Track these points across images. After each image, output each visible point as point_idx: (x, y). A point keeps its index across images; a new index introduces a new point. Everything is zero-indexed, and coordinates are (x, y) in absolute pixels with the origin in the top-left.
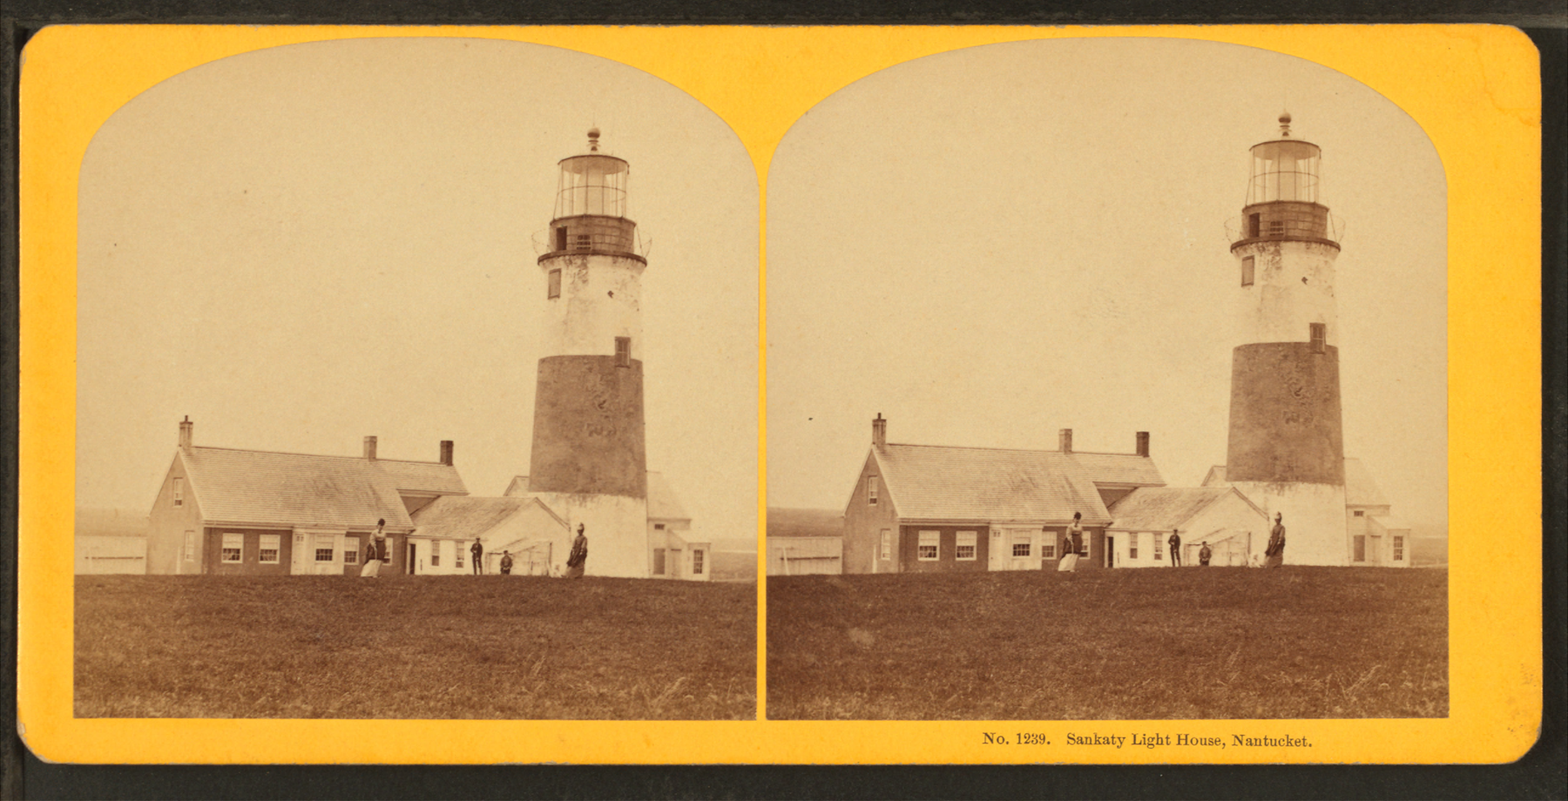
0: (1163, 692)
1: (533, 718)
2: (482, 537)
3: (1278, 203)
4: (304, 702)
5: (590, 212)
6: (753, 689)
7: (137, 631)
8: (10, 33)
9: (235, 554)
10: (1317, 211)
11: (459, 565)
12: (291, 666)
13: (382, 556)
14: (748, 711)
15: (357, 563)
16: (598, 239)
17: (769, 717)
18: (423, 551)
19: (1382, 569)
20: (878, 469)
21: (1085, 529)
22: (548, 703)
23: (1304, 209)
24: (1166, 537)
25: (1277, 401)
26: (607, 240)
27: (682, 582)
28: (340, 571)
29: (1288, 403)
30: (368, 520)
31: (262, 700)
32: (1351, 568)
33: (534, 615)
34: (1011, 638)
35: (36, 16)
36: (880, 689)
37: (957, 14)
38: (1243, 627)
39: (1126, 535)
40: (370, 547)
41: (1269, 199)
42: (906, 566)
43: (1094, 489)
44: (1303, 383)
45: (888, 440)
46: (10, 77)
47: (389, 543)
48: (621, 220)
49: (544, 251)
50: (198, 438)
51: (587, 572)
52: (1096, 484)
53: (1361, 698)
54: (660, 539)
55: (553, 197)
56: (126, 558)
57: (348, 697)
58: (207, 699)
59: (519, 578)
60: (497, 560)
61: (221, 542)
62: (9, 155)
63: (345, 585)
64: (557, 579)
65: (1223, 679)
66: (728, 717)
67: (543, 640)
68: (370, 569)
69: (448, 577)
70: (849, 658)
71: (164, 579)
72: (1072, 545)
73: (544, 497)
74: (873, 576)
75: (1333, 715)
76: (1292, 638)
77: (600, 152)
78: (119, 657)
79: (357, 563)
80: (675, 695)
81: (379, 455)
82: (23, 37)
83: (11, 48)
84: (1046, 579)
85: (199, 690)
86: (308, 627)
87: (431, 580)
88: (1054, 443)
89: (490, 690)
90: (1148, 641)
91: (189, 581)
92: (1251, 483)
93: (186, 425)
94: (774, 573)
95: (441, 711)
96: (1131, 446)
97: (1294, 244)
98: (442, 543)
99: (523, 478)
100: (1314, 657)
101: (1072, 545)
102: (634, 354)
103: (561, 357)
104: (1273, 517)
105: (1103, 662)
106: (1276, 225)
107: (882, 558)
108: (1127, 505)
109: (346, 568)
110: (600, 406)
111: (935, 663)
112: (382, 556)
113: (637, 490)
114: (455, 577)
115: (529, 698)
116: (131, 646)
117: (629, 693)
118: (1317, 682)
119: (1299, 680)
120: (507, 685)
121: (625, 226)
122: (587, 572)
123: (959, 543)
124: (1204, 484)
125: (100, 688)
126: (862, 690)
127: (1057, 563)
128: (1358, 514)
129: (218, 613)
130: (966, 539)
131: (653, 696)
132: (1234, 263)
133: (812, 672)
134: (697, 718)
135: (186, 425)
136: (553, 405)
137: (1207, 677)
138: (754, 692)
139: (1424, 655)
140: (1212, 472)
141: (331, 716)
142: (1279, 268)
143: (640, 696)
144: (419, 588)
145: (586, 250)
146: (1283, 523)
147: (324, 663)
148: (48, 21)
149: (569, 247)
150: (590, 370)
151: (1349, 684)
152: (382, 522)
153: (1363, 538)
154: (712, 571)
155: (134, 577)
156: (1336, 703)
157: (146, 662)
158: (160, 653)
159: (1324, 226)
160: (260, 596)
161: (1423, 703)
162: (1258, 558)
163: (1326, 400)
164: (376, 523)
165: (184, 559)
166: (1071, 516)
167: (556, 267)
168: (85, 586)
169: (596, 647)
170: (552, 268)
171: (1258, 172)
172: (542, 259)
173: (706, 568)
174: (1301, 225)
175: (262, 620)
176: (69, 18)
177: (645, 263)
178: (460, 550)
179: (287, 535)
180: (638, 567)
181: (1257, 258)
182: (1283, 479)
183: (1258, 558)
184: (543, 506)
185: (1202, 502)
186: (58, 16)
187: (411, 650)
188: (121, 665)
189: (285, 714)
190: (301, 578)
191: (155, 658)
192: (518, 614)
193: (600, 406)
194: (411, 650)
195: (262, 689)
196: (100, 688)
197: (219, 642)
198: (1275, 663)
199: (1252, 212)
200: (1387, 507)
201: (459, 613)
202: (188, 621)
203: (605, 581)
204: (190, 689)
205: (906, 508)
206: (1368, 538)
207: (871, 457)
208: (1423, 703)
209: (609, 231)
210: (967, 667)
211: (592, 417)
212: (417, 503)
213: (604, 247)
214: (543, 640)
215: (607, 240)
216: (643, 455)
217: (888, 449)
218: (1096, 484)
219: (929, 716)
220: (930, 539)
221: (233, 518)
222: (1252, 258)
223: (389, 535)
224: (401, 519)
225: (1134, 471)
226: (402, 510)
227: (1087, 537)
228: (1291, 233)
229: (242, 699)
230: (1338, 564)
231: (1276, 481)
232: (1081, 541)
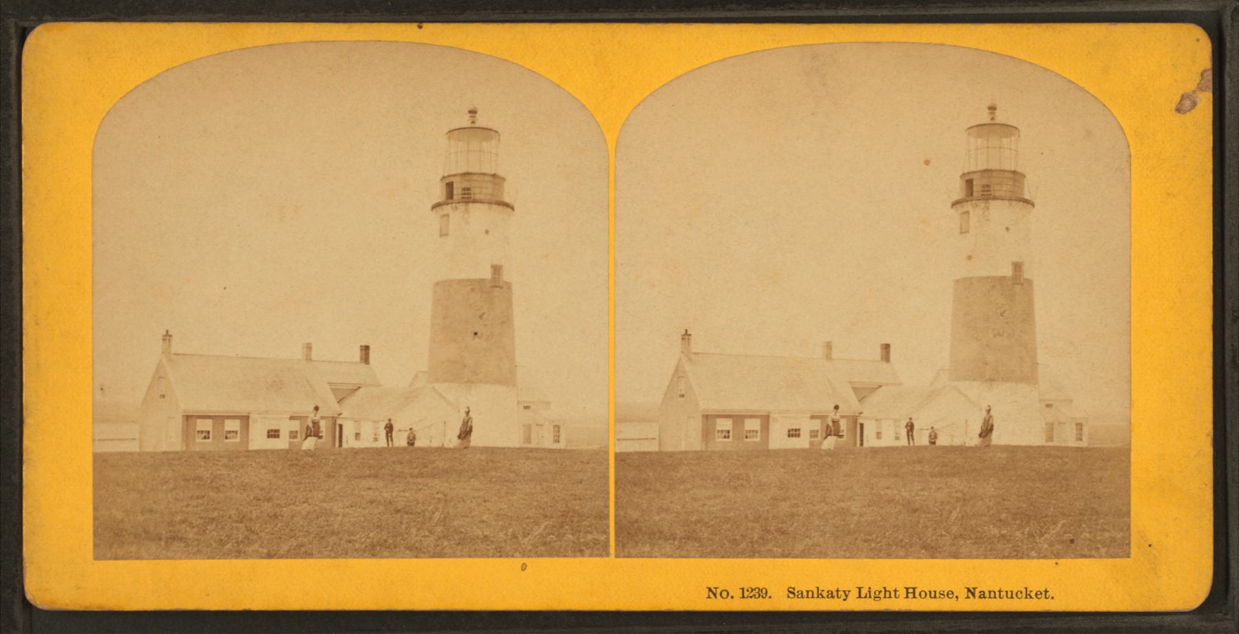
0: (901, 541)
1: (434, 556)
2: (914, 417)
5: (471, 170)
10: (1016, 176)
11: (376, 440)
12: (251, 520)
13: (317, 434)
15: (819, 439)
16: (477, 191)
17: (617, 556)
18: (348, 431)
21: (842, 417)
22: (446, 543)
23: (1006, 175)
24: (904, 423)
26: (484, 191)
28: (807, 446)
29: (1000, 311)
31: (228, 546)
33: (953, 475)
34: (269, 500)
36: (174, 539)
38: (962, 492)
39: (873, 422)
41: (980, 168)
43: (328, 388)
45: (173, 351)
47: (323, 424)
48: (1014, 172)
49: (957, 197)
52: (851, 383)
53: (1051, 544)
55: (437, 161)
57: (294, 542)
58: (187, 545)
60: (927, 433)
61: (195, 424)
62: (14, 123)
63: (291, 458)
64: (971, 448)
67: (440, 496)
69: (888, 448)
70: (663, 515)
71: (153, 455)
73: (441, 387)
74: (682, 453)
75: (1029, 557)
76: (480, 500)
77: (477, 125)
78: (119, 515)
79: (819, 439)
80: (541, 535)
81: (314, 357)
82: (23, 35)
83: (14, 42)
86: (262, 489)
87: (355, 452)
89: (401, 534)
90: (371, 502)
91: (172, 456)
92: (446, 384)
93: (167, 336)
94: (618, 450)
95: (365, 551)
96: (878, 353)
97: (998, 202)
100: (1015, 514)
101: (833, 430)
102: (506, 277)
105: (339, 518)
107: (687, 439)
108: (875, 398)
109: (290, 444)
110: (481, 317)
111: (729, 519)
112: (317, 434)
114: (551, 451)
118: (1018, 534)
120: (414, 531)
125: (112, 538)
126: (674, 539)
127: (301, 444)
129: (194, 480)
130: (752, 425)
131: (525, 536)
132: (434, 218)
135: (167, 336)
137: (418, 530)
139: (1097, 513)
140: (416, 376)
141: (282, 557)
143: (514, 536)
144: (346, 458)
145: (988, 195)
146: (992, 413)
148: (41, 21)
149: (455, 197)
151: (1042, 535)
152: (317, 408)
155: (130, 454)
156: (1032, 549)
158: (151, 511)
159: (1023, 188)
160: (225, 466)
161: (1097, 549)
162: (973, 440)
164: (832, 408)
165: (170, 439)
166: (311, 408)
167: (965, 209)
169: (480, 500)
172: (955, 204)
175: (227, 484)
177: (1033, 205)
179: (245, 419)
180: (1033, 437)
181: (452, 216)
182: (470, 382)
183: (973, 440)
186: (48, 17)
187: (340, 505)
188: (122, 521)
189: (761, 555)
190: (257, 452)
194: (340, 505)
195: (229, 537)
196: (112, 538)
197: (194, 503)
198: (986, 519)
199: (448, 181)
201: (376, 476)
204: (174, 538)
207: (680, 359)
208: (1097, 549)
211: (477, 315)
212: (344, 394)
215: (484, 191)
218: (851, 383)
220: (726, 424)
221: (203, 408)
222: (968, 212)
224: (330, 406)
226: (332, 400)
227: (843, 425)
228: (997, 194)
229: (214, 545)
230: (511, 445)
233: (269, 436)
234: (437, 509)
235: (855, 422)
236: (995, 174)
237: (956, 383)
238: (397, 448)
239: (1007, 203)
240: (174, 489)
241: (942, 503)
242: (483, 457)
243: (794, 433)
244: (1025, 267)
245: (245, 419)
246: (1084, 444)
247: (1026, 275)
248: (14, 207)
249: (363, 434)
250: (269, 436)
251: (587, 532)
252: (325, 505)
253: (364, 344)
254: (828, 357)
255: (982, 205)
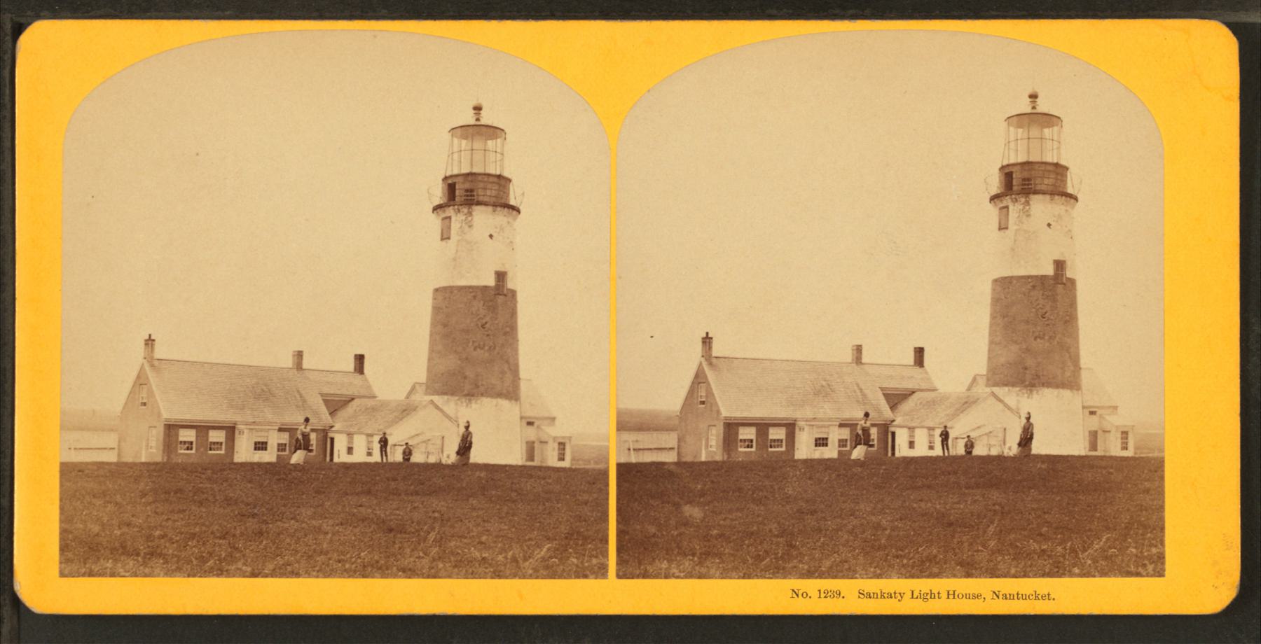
1: (428, 577)
2: (388, 432)
3: (1028, 163)
4: (244, 564)
5: (475, 170)
6: (605, 554)
7: (110, 507)
8: (8, 27)
9: (189, 445)
10: (1059, 170)
11: (369, 454)
12: (234, 535)
13: (307, 447)
14: (601, 572)
15: (287, 453)
16: (481, 192)
17: (619, 577)
18: (340, 443)
19: (1111, 457)
20: (706, 377)
21: (873, 425)
24: (938, 432)
25: (1027, 322)
26: (488, 193)
27: (549, 468)
29: (1036, 324)
30: (296, 418)
31: (211, 563)
32: (1086, 457)
34: (813, 513)
35: (29, 13)
36: (707, 554)
37: (769, 11)
39: (906, 430)
40: (297, 440)
41: (1020, 160)
42: (729, 455)
44: (1048, 308)
46: (9, 62)
47: (313, 436)
48: (499, 177)
49: (437, 201)
50: (160, 352)
51: (472, 460)
52: (882, 389)
53: (1095, 561)
54: (531, 434)
56: (101, 449)
57: (280, 561)
59: (417, 465)
61: (177, 435)
63: (277, 470)
64: (448, 466)
65: (984, 546)
66: (586, 577)
67: (436, 515)
68: (298, 457)
69: (360, 464)
70: (682, 529)
72: (862, 438)
75: (1072, 575)
76: (1039, 513)
77: (483, 122)
78: (96, 529)
79: (287, 453)
80: (543, 559)
81: (304, 366)
82: (19, 30)
83: (8, 38)
84: (841, 465)
85: (160, 555)
86: (248, 504)
87: (347, 467)
88: (848, 356)
89: (394, 555)
90: (923, 515)
92: (1006, 389)
94: (623, 460)
95: (355, 572)
96: (910, 358)
97: (1040, 197)
98: (355, 437)
99: (421, 384)
100: (1057, 528)
101: (862, 438)
102: (510, 285)
103: (451, 287)
104: (1024, 416)
105: (887, 532)
106: (1026, 181)
107: (709, 448)
109: (278, 457)
110: (483, 326)
112: (307, 447)
113: (512, 394)
115: (426, 561)
116: (105, 519)
117: (506, 558)
118: (1059, 549)
119: (1044, 547)
120: (408, 551)
121: (503, 182)
122: (472, 460)
123: (771, 437)
124: (969, 389)
125: (81, 553)
126: (694, 555)
127: (850, 453)
128: (1092, 413)
129: (176, 493)
130: (777, 434)
131: (525, 559)
132: (992, 211)
133: (653, 540)
134: (560, 577)
136: (445, 326)
138: (607, 556)
141: (266, 576)
142: (1028, 216)
143: (515, 560)
144: (337, 472)
145: (471, 201)
147: (261, 533)
148: (38, 17)
149: (457, 199)
150: (475, 297)
151: (1085, 550)
152: (307, 420)
153: (1096, 432)
154: (573, 459)
156: (1074, 565)
157: (118, 532)
158: (129, 525)
159: (1065, 184)
160: (209, 479)
161: (1144, 566)
162: (1012, 449)
163: (1066, 322)
164: (302, 420)
166: (861, 415)
168: (68, 471)
169: (479, 520)
170: (444, 215)
171: (1012, 138)
172: (436, 209)
173: (568, 457)
174: (1046, 181)
175: (211, 498)
176: (56, 15)
177: (519, 211)
178: (370, 442)
181: (1011, 208)
182: (1033, 385)
183: (1012, 449)
184: (437, 407)
185: (967, 404)
187: (331, 522)
189: (229, 574)
190: (243, 465)
191: (125, 529)
192: (417, 493)
193: (483, 326)
195: (211, 554)
196: (81, 553)
199: (1007, 171)
200: (1116, 408)
201: (369, 492)
202: (151, 499)
203: (486, 467)
204: (153, 554)
205: (729, 408)
206: (1100, 434)
207: (700, 368)
208: (1144, 566)
209: (489, 186)
210: (777, 536)
211: (476, 335)
213: (486, 199)
214: (436, 515)
215: (488, 193)
216: (517, 365)
217: (714, 361)
218: (882, 389)
219: (747, 576)
220: (748, 433)
222: (1007, 207)
223: (313, 430)
224: (323, 417)
225: (912, 379)
226: (324, 410)
227: (874, 432)
228: (1038, 188)
229: (195, 562)
230: (1076, 453)
231: (1026, 386)
232: (869, 435)
234: (433, 529)
235: (326, 437)
236: (1036, 167)
237: (436, 398)
238: (391, 464)
239: (1048, 197)
240: (711, 502)
241: (419, 523)
242: (483, 474)
243: (821, 442)
244: (510, 275)
245: (791, 427)
247: (1069, 274)
248: (7, 214)
249: (354, 448)
251: (1151, 545)
252: (873, 518)
253: (359, 352)
255: (465, 210)
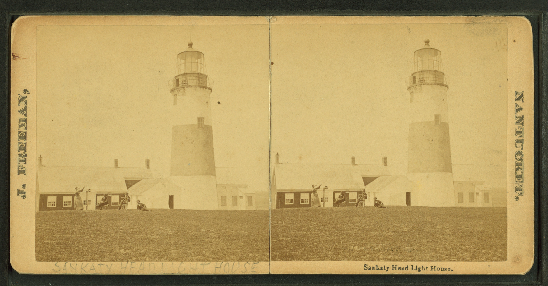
222: (413, 92)
233: (170, 196)
246: (253, 208)
250: (170, 196)
254: (116, 165)
